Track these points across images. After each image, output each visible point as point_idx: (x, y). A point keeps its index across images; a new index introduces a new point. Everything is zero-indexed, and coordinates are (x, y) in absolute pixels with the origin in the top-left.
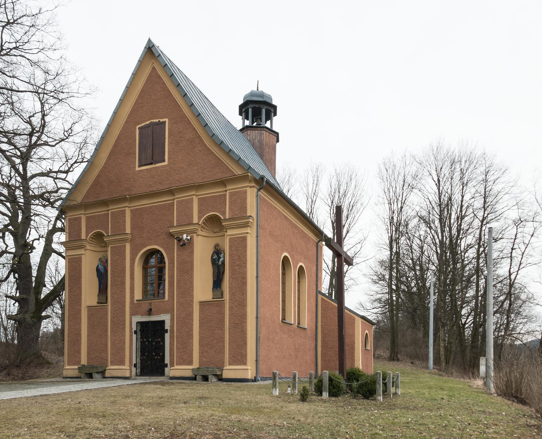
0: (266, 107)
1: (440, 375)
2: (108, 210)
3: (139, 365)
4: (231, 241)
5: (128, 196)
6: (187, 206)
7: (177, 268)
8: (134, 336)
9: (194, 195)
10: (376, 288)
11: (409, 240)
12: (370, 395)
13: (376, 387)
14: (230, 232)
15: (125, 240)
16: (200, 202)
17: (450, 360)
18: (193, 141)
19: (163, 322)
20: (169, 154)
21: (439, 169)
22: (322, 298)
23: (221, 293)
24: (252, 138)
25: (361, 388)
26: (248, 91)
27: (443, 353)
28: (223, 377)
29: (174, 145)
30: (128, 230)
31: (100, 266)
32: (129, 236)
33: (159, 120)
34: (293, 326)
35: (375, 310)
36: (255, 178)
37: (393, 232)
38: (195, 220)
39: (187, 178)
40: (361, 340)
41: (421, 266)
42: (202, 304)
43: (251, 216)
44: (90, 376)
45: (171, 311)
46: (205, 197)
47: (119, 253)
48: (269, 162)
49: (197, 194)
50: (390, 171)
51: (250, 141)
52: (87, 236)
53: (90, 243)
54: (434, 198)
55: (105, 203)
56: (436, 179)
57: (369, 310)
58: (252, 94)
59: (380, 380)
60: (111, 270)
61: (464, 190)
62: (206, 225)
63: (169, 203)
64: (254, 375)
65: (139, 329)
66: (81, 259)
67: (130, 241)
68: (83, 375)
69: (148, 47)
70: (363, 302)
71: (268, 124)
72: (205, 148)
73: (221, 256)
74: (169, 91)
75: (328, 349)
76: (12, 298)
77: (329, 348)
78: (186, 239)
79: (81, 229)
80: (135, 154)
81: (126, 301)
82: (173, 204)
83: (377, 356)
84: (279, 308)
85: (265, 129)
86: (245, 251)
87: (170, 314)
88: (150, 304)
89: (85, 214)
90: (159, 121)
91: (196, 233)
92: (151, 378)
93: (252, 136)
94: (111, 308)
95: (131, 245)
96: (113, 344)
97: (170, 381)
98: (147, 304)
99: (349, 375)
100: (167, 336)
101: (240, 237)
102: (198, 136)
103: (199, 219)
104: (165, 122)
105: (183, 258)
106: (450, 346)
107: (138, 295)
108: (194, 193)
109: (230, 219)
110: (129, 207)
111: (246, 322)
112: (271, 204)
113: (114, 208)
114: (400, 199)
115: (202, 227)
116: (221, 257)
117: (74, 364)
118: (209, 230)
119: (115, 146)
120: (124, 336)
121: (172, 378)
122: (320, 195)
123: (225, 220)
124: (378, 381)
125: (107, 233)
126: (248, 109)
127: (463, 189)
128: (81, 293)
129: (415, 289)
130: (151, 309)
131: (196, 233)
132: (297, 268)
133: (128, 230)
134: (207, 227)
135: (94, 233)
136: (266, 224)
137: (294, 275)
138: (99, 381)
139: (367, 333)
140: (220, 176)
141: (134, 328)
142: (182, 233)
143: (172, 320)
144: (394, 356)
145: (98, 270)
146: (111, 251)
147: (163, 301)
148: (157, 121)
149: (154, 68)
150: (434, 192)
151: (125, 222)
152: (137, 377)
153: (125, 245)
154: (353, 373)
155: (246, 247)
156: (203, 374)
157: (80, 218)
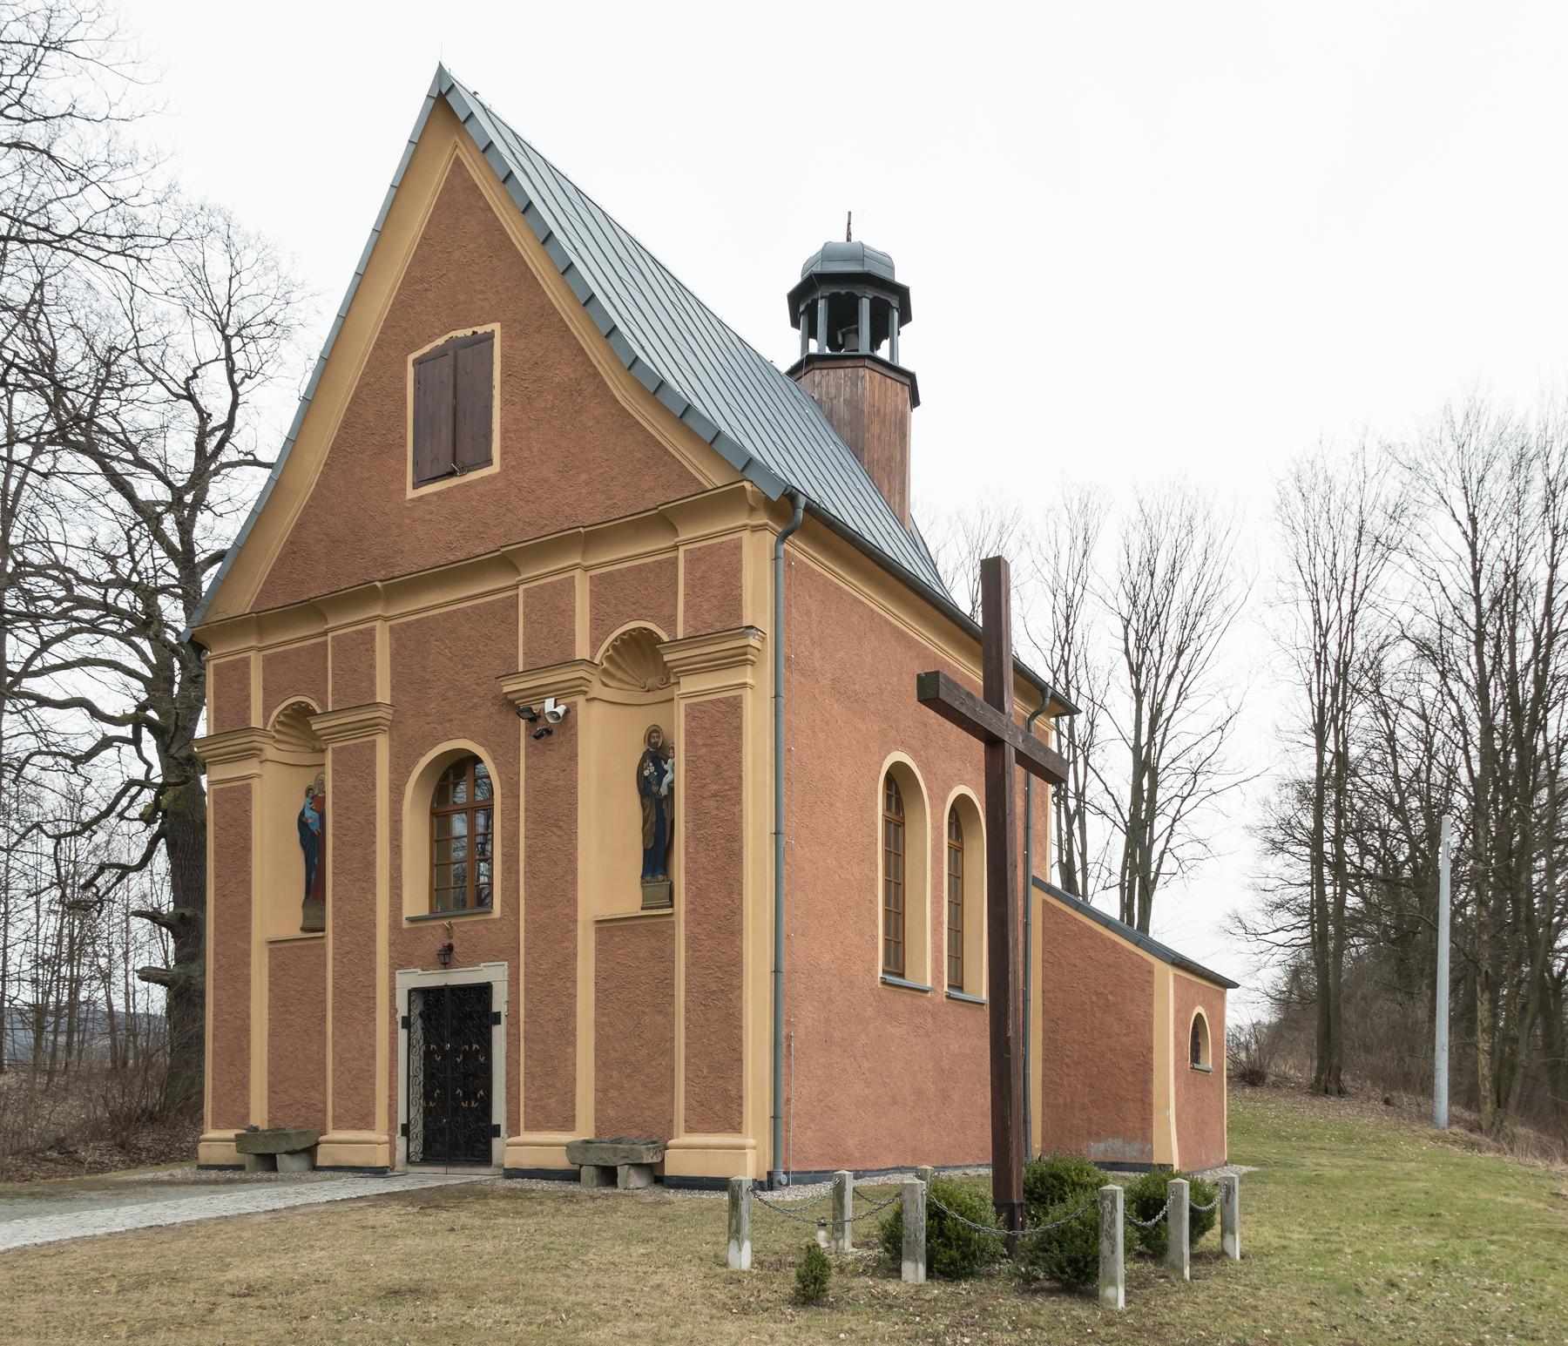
0: (871, 293)
1: (1472, 1145)
2: (325, 633)
3: (417, 1129)
4: (693, 713)
5: (378, 584)
6: (555, 605)
7: (526, 809)
8: (402, 1034)
9: (575, 567)
10: (1276, 864)
11: (1387, 717)
12: (1077, 1277)
13: (1098, 1251)
14: (689, 685)
15: (373, 727)
16: (596, 589)
17: (1512, 1095)
18: (577, 391)
19: (485, 990)
20: (503, 439)
21: (1474, 481)
22: (1045, 902)
23: (666, 889)
24: (827, 393)
25: (1046, 1251)
26: (814, 249)
27: (1486, 1071)
28: (667, 1173)
29: (518, 407)
30: (383, 694)
31: (308, 813)
32: (386, 713)
33: (475, 329)
34: (929, 995)
35: (1282, 937)
36: (768, 498)
37: (1325, 690)
38: (582, 650)
39: (558, 512)
40: (1176, 1037)
41: (1425, 798)
42: (607, 927)
43: (752, 627)
44: (268, 1162)
45: (508, 953)
46: (610, 574)
47: (358, 767)
48: (884, 469)
49: (586, 564)
50: (1316, 500)
51: (819, 403)
52: (266, 717)
53: (278, 741)
54: (1457, 579)
55: (313, 610)
56: (1463, 516)
57: (1263, 937)
58: (828, 253)
59: (1113, 1222)
60: (335, 822)
61: (1557, 549)
62: (619, 667)
63: (502, 600)
64: (768, 1168)
65: (417, 1012)
66: (250, 792)
67: (390, 728)
68: (247, 1160)
69: (435, 95)
70: (1243, 910)
71: (883, 352)
72: (613, 411)
73: (666, 767)
74: (503, 232)
75: (1065, 1068)
76: (154, 917)
77: (1068, 1066)
78: (552, 713)
79: (248, 698)
80: (404, 446)
81: (378, 922)
82: (512, 603)
83: (1273, 1078)
84: (875, 937)
85: (867, 363)
86: (738, 749)
87: (506, 963)
88: (449, 931)
89: (260, 649)
90: (474, 333)
91: (585, 693)
92: (451, 1170)
93: (827, 386)
94: (336, 948)
95: (392, 740)
96: (340, 1061)
97: (508, 1183)
98: (440, 931)
99: (1043, 1183)
100: (499, 1034)
101: (719, 700)
102: (590, 370)
103: (595, 645)
104: (490, 337)
105: (544, 777)
106: (1511, 1048)
107: (416, 902)
108: (578, 561)
109: (691, 640)
110: (386, 619)
111: (740, 988)
112: (838, 588)
113: (343, 624)
114: (1349, 586)
115: (606, 672)
116: (666, 772)
117: (230, 1126)
118: (627, 683)
119: (346, 425)
120: (372, 1034)
121: (511, 1174)
122: (1093, 582)
123: (675, 643)
124: (1106, 1226)
125: (323, 704)
126: (815, 302)
127: (1554, 545)
128: (249, 900)
129: (1407, 872)
130: (450, 948)
131: (585, 693)
132: (945, 801)
133: (383, 694)
134: (624, 671)
135: (286, 709)
136: (817, 654)
137: (933, 827)
138: (300, 1181)
139: (1199, 1016)
140: (656, 498)
141: (402, 1011)
142: (540, 694)
143: (513, 981)
144: (1327, 1081)
145: (303, 824)
146: (333, 761)
147: (486, 921)
148: (468, 332)
149: (458, 163)
150: (1452, 557)
151: (372, 667)
152: (411, 1169)
153: (375, 741)
154: (1055, 1176)
155: (741, 734)
156: (600, 1163)
157: (246, 662)
